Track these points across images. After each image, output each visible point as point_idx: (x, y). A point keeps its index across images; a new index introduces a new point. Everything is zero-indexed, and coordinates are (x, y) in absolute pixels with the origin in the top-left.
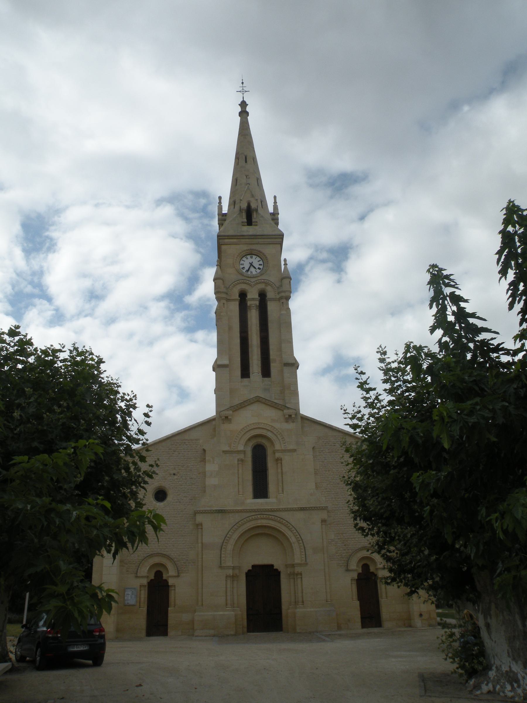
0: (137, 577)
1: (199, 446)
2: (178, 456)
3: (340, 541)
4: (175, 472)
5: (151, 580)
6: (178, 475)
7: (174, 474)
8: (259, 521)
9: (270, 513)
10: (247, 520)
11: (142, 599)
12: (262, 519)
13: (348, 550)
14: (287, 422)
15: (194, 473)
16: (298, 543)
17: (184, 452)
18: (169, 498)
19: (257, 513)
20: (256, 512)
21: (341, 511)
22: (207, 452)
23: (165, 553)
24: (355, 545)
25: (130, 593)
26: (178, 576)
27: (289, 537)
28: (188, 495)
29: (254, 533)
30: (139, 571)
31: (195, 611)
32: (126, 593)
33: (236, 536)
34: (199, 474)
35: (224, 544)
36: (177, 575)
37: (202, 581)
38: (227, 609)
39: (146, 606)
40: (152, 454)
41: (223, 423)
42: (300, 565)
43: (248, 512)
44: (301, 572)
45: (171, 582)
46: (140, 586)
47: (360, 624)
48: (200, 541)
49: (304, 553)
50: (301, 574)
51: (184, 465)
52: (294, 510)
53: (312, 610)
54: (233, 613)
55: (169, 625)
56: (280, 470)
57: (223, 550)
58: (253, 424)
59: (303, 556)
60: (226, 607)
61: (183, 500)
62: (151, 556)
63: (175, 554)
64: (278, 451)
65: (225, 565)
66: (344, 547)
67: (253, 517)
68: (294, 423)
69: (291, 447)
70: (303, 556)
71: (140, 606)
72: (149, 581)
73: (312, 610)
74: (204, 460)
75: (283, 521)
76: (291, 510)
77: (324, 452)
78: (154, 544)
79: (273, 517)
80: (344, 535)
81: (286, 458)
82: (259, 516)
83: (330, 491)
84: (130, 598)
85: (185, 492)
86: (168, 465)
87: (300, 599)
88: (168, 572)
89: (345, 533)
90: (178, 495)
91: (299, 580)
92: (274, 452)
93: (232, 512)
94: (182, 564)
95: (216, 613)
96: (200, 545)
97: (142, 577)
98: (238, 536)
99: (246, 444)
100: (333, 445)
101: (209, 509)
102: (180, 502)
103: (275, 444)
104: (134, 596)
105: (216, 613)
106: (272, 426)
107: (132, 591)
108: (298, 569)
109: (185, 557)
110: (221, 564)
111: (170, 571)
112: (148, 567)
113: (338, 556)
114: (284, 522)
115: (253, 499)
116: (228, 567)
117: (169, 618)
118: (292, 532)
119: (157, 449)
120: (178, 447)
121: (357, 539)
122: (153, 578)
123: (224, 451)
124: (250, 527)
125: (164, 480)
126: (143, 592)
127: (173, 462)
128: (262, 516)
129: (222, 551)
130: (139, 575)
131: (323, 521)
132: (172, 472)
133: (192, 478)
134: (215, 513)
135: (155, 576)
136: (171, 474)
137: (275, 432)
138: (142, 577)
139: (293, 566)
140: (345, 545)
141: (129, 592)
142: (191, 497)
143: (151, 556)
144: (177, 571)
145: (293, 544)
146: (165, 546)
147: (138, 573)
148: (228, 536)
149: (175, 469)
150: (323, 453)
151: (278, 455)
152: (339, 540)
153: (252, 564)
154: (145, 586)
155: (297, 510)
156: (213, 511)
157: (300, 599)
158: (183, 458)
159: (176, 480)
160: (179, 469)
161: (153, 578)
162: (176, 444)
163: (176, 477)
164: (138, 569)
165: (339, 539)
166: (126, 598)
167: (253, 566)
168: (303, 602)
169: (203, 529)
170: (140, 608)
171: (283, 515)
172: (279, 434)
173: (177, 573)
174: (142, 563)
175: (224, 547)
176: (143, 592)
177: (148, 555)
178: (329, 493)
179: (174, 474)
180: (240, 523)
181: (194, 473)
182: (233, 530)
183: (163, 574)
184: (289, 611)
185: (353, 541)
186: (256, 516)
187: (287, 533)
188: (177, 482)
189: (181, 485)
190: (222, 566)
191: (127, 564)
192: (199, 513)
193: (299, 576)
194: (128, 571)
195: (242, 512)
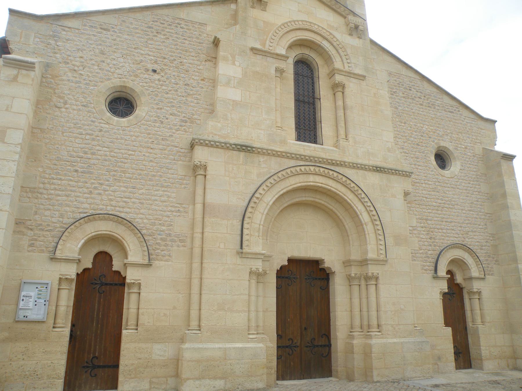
0: (53, 259)
1: (205, 35)
2: (164, 42)
3: (424, 231)
4: (156, 67)
5: (86, 270)
6: (163, 74)
7: (154, 71)
8: (311, 178)
9: (332, 168)
10: (291, 172)
11: (62, 309)
12: (316, 174)
13: (435, 246)
14: (351, 35)
15: (193, 77)
16: (373, 223)
17: (177, 38)
18: (140, 112)
19: (310, 164)
20: (306, 160)
21: (424, 185)
22: (221, 44)
23: (122, 215)
24: (443, 239)
25: (32, 294)
26: (149, 265)
27: (359, 214)
28: (179, 112)
29: (297, 200)
30: (59, 247)
31: (182, 340)
32: (23, 293)
33: (270, 198)
34: (202, 80)
35: (250, 210)
36: (146, 262)
37: (201, 279)
38: (251, 336)
39: (69, 325)
40: (113, 28)
41: (253, 7)
42: (377, 262)
43: (292, 158)
44: (378, 274)
45: (131, 275)
46: (60, 279)
47: (454, 364)
48: (199, 199)
49: (382, 243)
50: (377, 278)
51: (175, 60)
52: (366, 169)
53: (395, 340)
54: (261, 345)
55: (121, 368)
56: (340, 103)
57: (246, 220)
58: (302, 21)
59: (381, 247)
60: (249, 334)
61: (167, 119)
62: (91, 218)
63: (145, 221)
64: (340, 72)
65: (250, 251)
66: (429, 240)
67: (303, 168)
68: (361, 40)
69: (358, 71)
70: (381, 247)
71: (54, 323)
72: (80, 271)
73: (395, 340)
74: (214, 59)
75: (350, 184)
76: (362, 169)
77: (398, 95)
78: (100, 194)
79: (335, 174)
80: (429, 222)
81: (352, 86)
82: (312, 168)
83: (408, 152)
84: (31, 305)
85: (173, 106)
86: (143, 52)
87: (374, 322)
88: (126, 255)
89: (431, 220)
90: (158, 108)
91: (372, 289)
92: (331, 74)
93: (264, 154)
94: (158, 241)
95: (228, 345)
96: (199, 207)
97: (68, 260)
98: (274, 199)
99: (291, 47)
100: (408, 88)
101: (222, 140)
102: (162, 122)
103: (128, 249)
104: (43, 301)
105: (228, 345)
106: (331, 34)
107: (40, 291)
108: (372, 270)
109: (164, 228)
110: (241, 247)
111: (130, 253)
112: (83, 241)
113: (422, 253)
114: (353, 185)
115: (296, 140)
116: (256, 256)
117: (122, 353)
118: (363, 204)
119: (124, 21)
120: (166, 28)
121: (445, 231)
122: (90, 266)
123: (252, 49)
124: (295, 186)
125: (133, 78)
126: (64, 294)
127: (154, 50)
128: (317, 169)
129: (245, 222)
130: (58, 254)
131: (406, 194)
132: (150, 67)
133: (187, 85)
134: (233, 149)
135: (94, 263)
136: (147, 70)
137: (335, 44)
138: (68, 260)
139: (364, 262)
140: (431, 238)
141: (31, 292)
142: (184, 117)
143: (91, 218)
144: (146, 253)
145: (365, 226)
146: (125, 202)
147: (57, 252)
148: (257, 195)
149: (156, 62)
150: (397, 96)
151: (338, 78)
152: (423, 229)
153: (289, 256)
154: (72, 280)
155: (370, 170)
156: (231, 145)
157: (374, 322)
158: (173, 46)
159: (156, 82)
160: (165, 65)
161: (90, 266)
162: (162, 22)
163: (156, 76)
164: (58, 243)
165: (422, 227)
166: (21, 304)
167: (290, 260)
168: (379, 326)
169: (207, 177)
170: (54, 327)
171: (350, 173)
172: (341, 48)
173: (147, 258)
174: (69, 230)
175: (248, 215)
176: (64, 294)
177: (85, 215)
178: (407, 155)
179: (154, 71)
180: (280, 175)
181: (193, 77)
182: (267, 186)
183: (113, 260)
184: (355, 342)
185: (440, 234)
186: (307, 168)
187: (355, 205)
188: (159, 86)
189: (167, 93)
190: (244, 251)
191: (31, 229)
192: (201, 144)
193: (136, 290)
194: (31, 245)
195: (283, 157)
